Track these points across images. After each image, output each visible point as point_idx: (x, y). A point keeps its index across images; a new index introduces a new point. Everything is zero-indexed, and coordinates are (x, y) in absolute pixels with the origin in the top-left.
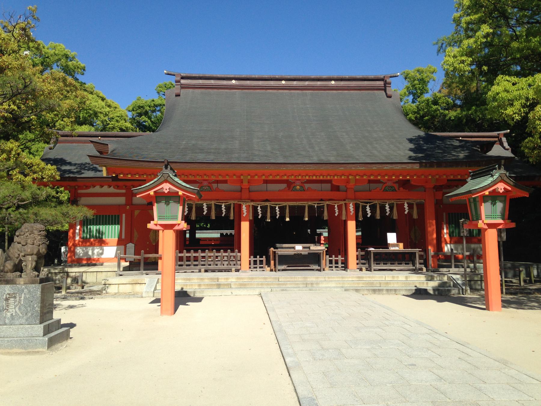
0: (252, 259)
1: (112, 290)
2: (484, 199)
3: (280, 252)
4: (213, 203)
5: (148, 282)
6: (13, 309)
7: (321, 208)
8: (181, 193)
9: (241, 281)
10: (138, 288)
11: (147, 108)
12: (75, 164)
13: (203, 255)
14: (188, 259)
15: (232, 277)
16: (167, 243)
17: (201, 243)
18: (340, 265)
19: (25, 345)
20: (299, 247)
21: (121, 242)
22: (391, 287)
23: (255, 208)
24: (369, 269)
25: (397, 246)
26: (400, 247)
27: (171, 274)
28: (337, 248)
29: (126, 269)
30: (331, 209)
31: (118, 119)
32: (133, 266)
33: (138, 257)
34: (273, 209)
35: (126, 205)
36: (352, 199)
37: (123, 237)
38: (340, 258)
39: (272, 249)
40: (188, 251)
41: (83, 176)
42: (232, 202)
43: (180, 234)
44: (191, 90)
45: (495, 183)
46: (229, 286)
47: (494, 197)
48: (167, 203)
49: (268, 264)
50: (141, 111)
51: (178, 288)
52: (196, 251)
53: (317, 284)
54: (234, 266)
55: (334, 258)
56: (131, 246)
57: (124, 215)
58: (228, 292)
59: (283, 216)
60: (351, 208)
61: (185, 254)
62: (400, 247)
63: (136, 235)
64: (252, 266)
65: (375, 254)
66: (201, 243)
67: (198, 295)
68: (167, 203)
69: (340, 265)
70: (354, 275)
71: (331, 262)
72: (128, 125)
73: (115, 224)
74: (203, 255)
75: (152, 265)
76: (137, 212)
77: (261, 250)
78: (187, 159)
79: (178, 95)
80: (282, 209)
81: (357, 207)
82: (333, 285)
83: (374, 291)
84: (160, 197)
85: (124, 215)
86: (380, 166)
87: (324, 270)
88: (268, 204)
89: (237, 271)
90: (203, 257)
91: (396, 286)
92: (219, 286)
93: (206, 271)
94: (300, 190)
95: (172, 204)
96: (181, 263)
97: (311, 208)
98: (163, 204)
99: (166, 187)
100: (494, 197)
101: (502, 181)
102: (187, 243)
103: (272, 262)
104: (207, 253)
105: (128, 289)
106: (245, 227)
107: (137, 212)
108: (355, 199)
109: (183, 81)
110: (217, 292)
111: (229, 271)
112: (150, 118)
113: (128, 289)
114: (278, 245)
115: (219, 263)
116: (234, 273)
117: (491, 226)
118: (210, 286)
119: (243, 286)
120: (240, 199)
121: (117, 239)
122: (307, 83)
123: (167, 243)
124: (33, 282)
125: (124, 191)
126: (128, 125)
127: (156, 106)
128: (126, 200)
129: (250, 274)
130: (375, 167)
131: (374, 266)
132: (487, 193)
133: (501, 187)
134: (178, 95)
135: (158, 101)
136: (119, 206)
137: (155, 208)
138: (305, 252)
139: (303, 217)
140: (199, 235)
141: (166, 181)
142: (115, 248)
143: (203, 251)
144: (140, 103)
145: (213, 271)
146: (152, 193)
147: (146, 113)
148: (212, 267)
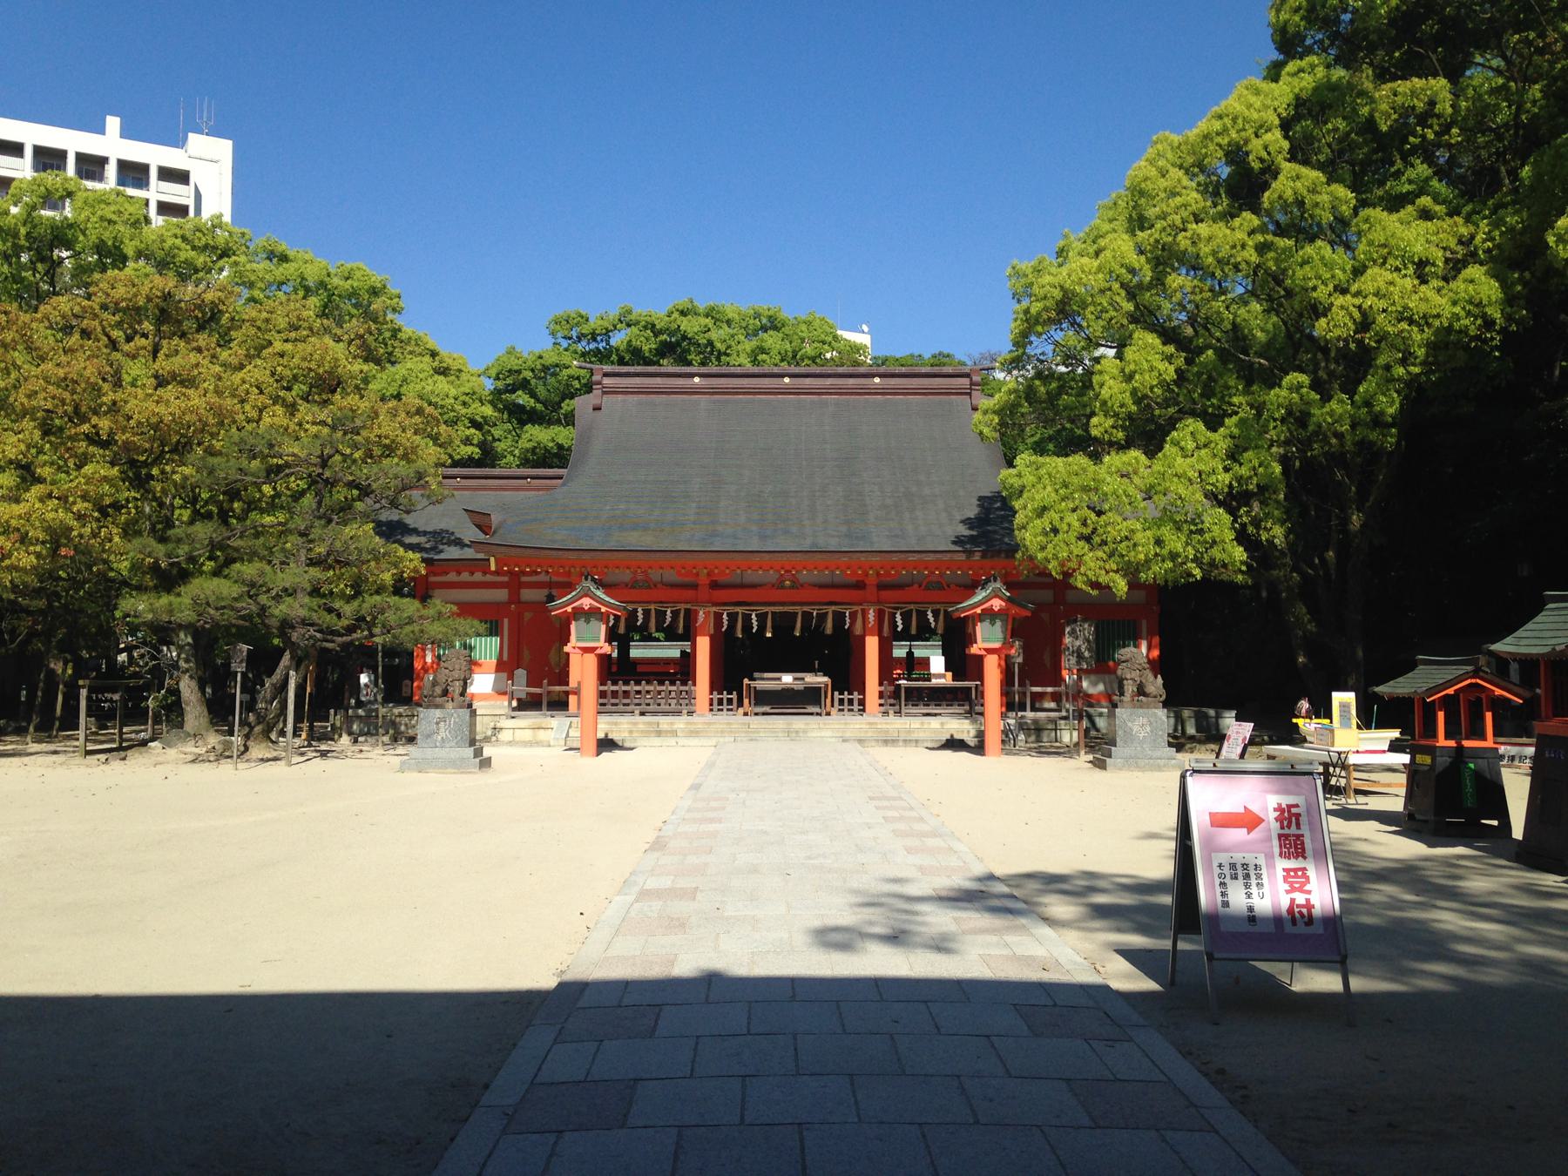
0: (716, 696)
1: (505, 736)
2: (980, 618)
3: (760, 685)
4: (652, 607)
5: (555, 726)
6: (443, 733)
7: (822, 617)
8: (603, 609)
9: (692, 727)
10: (542, 735)
11: (528, 374)
12: (425, 533)
13: (638, 688)
14: (615, 694)
15: (680, 722)
16: (583, 673)
17: (640, 669)
18: (856, 707)
19: (458, 766)
20: (787, 679)
21: (501, 667)
22: (914, 736)
23: (718, 616)
24: (898, 713)
25: (943, 676)
26: (947, 680)
27: (585, 716)
28: (847, 680)
29: (514, 709)
30: (839, 618)
31: (467, 399)
32: (528, 704)
33: (538, 690)
34: (747, 618)
35: (510, 603)
36: (873, 603)
37: (505, 657)
38: (856, 696)
39: (746, 681)
40: (615, 683)
41: (442, 556)
42: (682, 607)
43: (604, 660)
44: (620, 397)
45: (987, 599)
46: (674, 733)
47: (990, 615)
48: (588, 621)
49: (740, 704)
50: (512, 381)
51: (601, 735)
52: (626, 683)
53: (805, 732)
54: (685, 704)
55: (846, 696)
56: (521, 674)
57: (506, 621)
58: (672, 741)
59: (762, 628)
60: (871, 616)
61: (609, 687)
62: (947, 680)
63: (526, 655)
64: (715, 707)
65: (907, 689)
66: (640, 669)
67: (627, 745)
68: (588, 621)
69: (856, 707)
70: (874, 720)
71: (841, 702)
72: (488, 411)
73: (491, 635)
74: (638, 688)
75: (559, 704)
76: (528, 616)
77: (731, 681)
78: (612, 545)
79: (597, 408)
80: (762, 618)
81: (880, 615)
82: (829, 733)
83: (886, 742)
84: (579, 613)
85: (506, 621)
86: (903, 556)
87: (828, 714)
88: (739, 609)
89: (690, 713)
90: (638, 692)
91: (921, 735)
92: (659, 733)
93: (642, 714)
94: (792, 587)
95: (594, 623)
96: (607, 702)
97: (807, 616)
98: (582, 622)
99: (586, 603)
100: (990, 615)
101: (996, 596)
102: (614, 669)
103: (746, 701)
104: (644, 687)
105: (527, 735)
106: (703, 645)
107: (528, 616)
108: (879, 602)
109: (606, 381)
110: (657, 741)
111: (679, 713)
112: (533, 395)
113: (527, 735)
114: (756, 675)
115: (673, 702)
116: (685, 718)
117: (990, 651)
118: (646, 734)
119: (694, 733)
120: (696, 602)
121: (494, 661)
122: (829, 381)
123: (583, 673)
124: (461, 707)
125: (506, 579)
126: (488, 411)
127: (545, 368)
128: (510, 594)
129: (709, 717)
130: (895, 558)
131: (904, 710)
132: (979, 611)
133: (997, 604)
134: (597, 408)
135: (551, 359)
136: (498, 604)
137: (573, 627)
138: (799, 686)
139: (793, 628)
140: (636, 652)
141: (586, 595)
142: (492, 676)
143: (638, 683)
144: (514, 364)
145: (655, 713)
146: (569, 609)
147: (524, 385)
148: (651, 708)
